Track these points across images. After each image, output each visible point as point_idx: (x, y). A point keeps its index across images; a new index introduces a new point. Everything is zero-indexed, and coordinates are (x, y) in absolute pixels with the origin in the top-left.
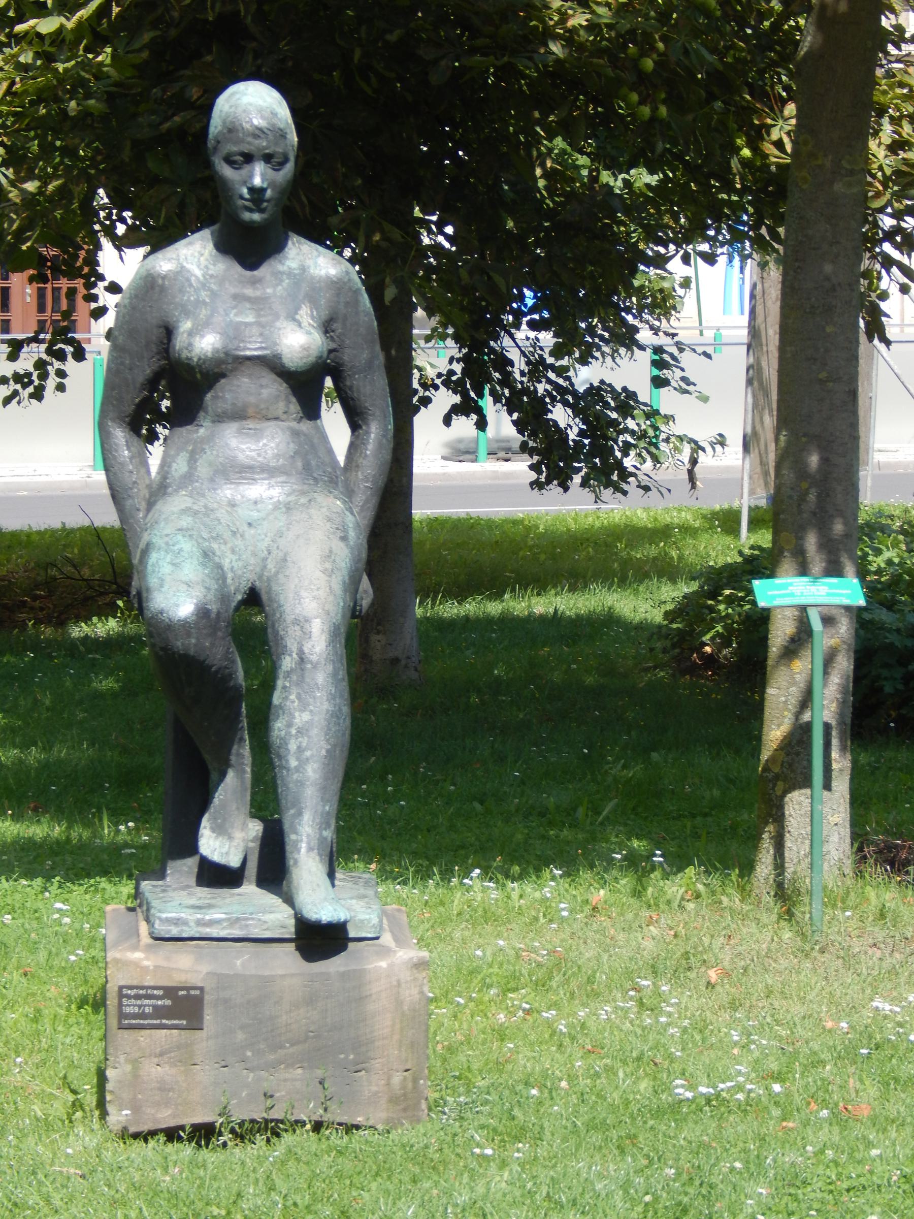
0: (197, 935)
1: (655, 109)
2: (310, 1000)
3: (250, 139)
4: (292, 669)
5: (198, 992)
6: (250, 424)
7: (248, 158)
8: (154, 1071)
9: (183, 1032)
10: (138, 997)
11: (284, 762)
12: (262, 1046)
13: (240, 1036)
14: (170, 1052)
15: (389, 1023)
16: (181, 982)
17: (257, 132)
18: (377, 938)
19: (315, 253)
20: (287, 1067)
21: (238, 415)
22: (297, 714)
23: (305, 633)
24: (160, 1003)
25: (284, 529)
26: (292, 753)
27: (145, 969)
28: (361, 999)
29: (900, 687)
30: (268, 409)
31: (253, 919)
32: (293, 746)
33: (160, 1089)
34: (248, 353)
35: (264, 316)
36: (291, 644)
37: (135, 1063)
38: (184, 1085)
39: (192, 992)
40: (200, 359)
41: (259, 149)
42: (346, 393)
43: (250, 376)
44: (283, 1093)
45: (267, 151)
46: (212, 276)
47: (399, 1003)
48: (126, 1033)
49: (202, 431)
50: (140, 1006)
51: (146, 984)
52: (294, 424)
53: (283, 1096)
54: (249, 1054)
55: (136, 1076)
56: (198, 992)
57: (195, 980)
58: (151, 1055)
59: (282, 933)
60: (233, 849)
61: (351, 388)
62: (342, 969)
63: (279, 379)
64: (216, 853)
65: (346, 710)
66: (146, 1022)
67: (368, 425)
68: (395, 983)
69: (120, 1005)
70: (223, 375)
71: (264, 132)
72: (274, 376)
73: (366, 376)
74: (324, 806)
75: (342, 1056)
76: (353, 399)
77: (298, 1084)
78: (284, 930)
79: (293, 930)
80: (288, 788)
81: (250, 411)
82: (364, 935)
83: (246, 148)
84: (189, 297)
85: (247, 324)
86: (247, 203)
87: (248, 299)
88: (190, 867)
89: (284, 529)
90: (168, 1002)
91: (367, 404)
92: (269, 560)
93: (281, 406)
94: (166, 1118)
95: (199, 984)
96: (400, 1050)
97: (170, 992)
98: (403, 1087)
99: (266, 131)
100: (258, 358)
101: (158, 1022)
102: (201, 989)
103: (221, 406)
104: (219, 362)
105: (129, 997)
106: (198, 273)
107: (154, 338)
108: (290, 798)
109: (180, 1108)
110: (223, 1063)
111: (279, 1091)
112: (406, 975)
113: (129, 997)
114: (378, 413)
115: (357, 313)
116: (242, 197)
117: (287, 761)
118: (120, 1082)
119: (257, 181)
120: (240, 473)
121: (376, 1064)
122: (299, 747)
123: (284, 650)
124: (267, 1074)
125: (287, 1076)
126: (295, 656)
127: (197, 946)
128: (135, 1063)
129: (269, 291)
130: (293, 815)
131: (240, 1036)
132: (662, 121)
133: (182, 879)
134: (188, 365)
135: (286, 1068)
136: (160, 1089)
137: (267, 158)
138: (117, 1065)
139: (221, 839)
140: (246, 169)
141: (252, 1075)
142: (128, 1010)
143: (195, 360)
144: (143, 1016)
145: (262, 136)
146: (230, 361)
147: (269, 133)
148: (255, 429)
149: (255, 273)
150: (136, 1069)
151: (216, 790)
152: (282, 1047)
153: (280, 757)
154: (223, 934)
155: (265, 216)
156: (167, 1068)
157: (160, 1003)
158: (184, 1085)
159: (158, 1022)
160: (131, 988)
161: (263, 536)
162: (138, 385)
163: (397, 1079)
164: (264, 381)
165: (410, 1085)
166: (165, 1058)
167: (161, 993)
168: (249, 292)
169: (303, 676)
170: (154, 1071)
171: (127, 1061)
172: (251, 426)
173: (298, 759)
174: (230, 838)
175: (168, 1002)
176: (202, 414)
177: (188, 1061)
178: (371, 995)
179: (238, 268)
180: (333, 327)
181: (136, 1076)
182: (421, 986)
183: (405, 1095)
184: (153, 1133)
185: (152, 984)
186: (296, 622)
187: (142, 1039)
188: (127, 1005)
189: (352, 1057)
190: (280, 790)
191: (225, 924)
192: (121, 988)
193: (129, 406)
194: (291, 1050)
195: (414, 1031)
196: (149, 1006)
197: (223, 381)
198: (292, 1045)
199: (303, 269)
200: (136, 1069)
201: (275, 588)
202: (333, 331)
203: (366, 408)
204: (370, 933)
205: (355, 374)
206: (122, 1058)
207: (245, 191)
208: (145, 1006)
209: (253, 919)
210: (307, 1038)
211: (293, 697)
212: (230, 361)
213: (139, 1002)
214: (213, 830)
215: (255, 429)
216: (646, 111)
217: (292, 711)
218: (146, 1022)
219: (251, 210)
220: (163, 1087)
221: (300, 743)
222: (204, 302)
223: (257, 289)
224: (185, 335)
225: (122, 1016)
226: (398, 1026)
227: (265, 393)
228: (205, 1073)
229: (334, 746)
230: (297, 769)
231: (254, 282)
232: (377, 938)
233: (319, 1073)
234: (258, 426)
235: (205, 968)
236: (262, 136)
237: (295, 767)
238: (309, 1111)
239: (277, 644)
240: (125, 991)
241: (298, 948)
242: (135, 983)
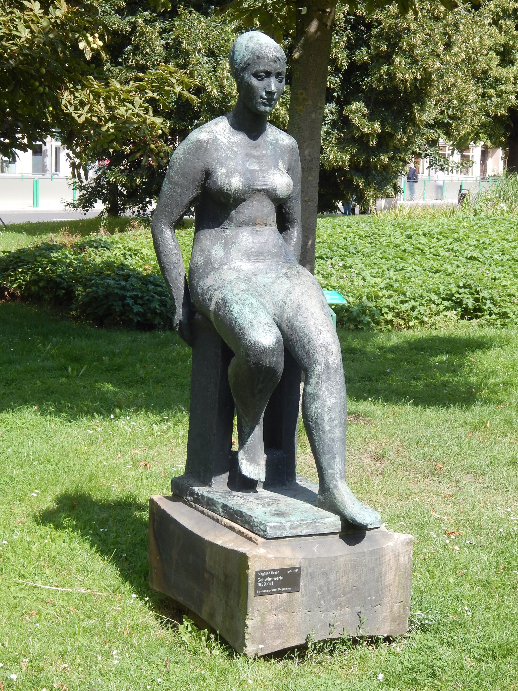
0: (290, 535)
1: (44, 89)
2: (355, 568)
3: (271, 63)
4: (322, 373)
5: (297, 570)
6: (257, 228)
7: (268, 74)
8: (272, 619)
9: (288, 594)
10: (266, 577)
11: (321, 428)
12: (329, 598)
13: (318, 593)
14: (282, 606)
15: (393, 577)
16: (288, 565)
17: (276, 59)
18: (379, 528)
19: (278, 132)
21: (251, 223)
22: (328, 399)
23: (329, 352)
24: (277, 579)
25: (291, 289)
26: (326, 422)
27: (270, 559)
28: (380, 565)
29: (122, 309)
31: (319, 522)
32: (326, 418)
33: (275, 629)
34: (259, 188)
35: (263, 166)
36: (321, 359)
37: (263, 615)
38: (288, 625)
39: (295, 571)
40: (235, 191)
41: (275, 70)
42: (286, 210)
44: (339, 623)
46: (233, 143)
47: (398, 565)
48: (258, 598)
49: (228, 232)
50: (266, 582)
51: (270, 568)
53: (339, 625)
54: (322, 602)
55: (263, 623)
56: (297, 570)
57: (296, 563)
58: (271, 610)
59: (334, 530)
60: (261, 471)
61: (289, 208)
62: (371, 549)
63: (272, 202)
64: (252, 474)
66: (270, 591)
67: (293, 228)
68: (397, 554)
69: (256, 582)
70: (245, 200)
71: (279, 60)
75: (369, 598)
76: (289, 214)
77: (347, 617)
78: (335, 528)
79: (340, 527)
80: (324, 442)
81: (258, 221)
82: (374, 527)
83: (268, 68)
84: (221, 155)
85: (255, 171)
86: (264, 101)
87: (254, 156)
88: (224, 479)
89: (291, 289)
90: (282, 578)
92: (286, 307)
94: (278, 645)
95: (298, 566)
96: (398, 592)
97: (283, 572)
98: (399, 612)
99: (280, 59)
100: (263, 190)
101: (276, 590)
102: (299, 568)
103: (242, 218)
104: (245, 192)
105: (261, 577)
106: (225, 141)
107: (198, 178)
108: (326, 448)
109: (286, 638)
110: (309, 610)
111: (337, 622)
112: (402, 549)
113: (261, 577)
116: (262, 97)
117: (323, 427)
118: (254, 627)
119: (273, 88)
120: (257, 256)
121: (386, 600)
122: (330, 419)
123: (316, 362)
124: (331, 613)
125: (342, 613)
126: (323, 365)
127: (289, 541)
128: (263, 615)
129: (264, 152)
130: (329, 458)
131: (318, 593)
132: (46, 94)
133: (221, 486)
134: (228, 194)
136: (275, 629)
138: (253, 618)
139: (253, 465)
140: (266, 81)
141: (323, 614)
142: (260, 585)
143: (233, 191)
144: (268, 587)
145: (278, 62)
148: (259, 231)
150: (263, 618)
151: (249, 437)
152: (340, 597)
153: (317, 424)
154: (304, 533)
156: (279, 616)
157: (277, 579)
158: (288, 625)
159: (276, 590)
160: (262, 572)
161: (278, 293)
162: (184, 204)
163: (396, 608)
164: (265, 204)
165: (402, 610)
166: (279, 610)
167: (278, 573)
168: (254, 152)
169: (329, 377)
170: (272, 619)
171: (259, 615)
172: (257, 229)
173: (330, 425)
174: (258, 464)
175: (282, 578)
176: (227, 222)
177: (290, 610)
179: (247, 138)
181: (263, 623)
182: (409, 555)
183: (399, 616)
184: (269, 655)
185: (273, 568)
186: (322, 345)
187: (267, 601)
188: (260, 582)
189: (374, 598)
190: (317, 443)
191: (304, 527)
192: (257, 572)
193: (176, 216)
194: (344, 598)
195: (405, 580)
196: (271, 581)
197: (244, 203)
198: (344, 595)
199: (276, 140)
200: (263, 618)
201: (296, 324)
206: (256, 613)
207: (264, 93)
208: (269, 581)
209: (319, 522)
210: (352, 590)
211: (324, 389)
213: (266, 580)
214: (248, 460)
215: (259, 231)
216: (41, 89)
217: (325, 397)
218: (270, 591)
219: (265, 105)
220: (277, 627)
221: (331, 416)
222: (231, 158)
223: (258, 151)
224: (224, 177)
225: (257, 588)
226: (397, 578)
227: (266, 210)
228: (299, 617)
230: (330, 432)
231: (256, 147)
232: (379, 528)
233: (358, 609)
234: (261, 229)
235: (300, 555)
236: (278, 62)
237: (329, 430)
238: (352, 632)
239: (309, 357)
240: (259, 574)
241: (341, 537)
242: (264, 568)
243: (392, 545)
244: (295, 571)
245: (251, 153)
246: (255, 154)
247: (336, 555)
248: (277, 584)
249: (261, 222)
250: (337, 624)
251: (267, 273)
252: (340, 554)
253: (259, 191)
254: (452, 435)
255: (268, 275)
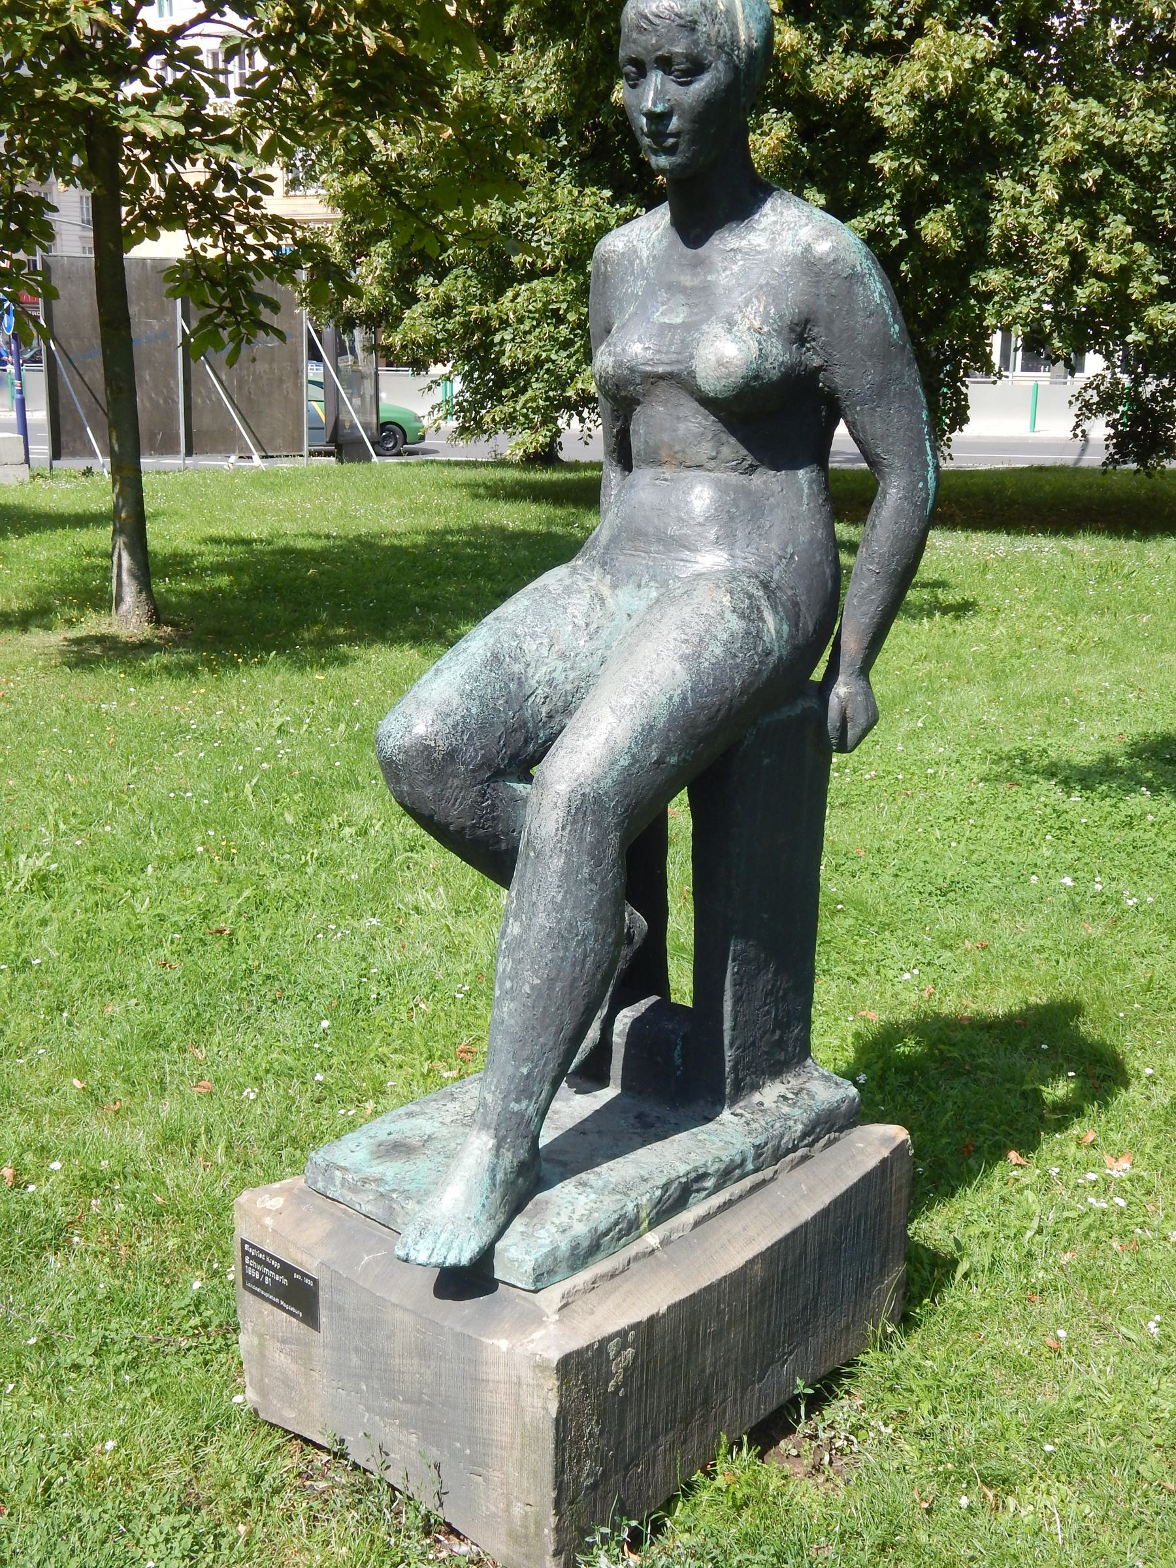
20: (401, 1425)
28: (478, 1381)
30: (684, 452)
39: (307, 1281)
43: (665, 403)
45: (660, 53)
50: (261, 1273)
52: (734, 478)
63: (702, 409)
65: (586, 926)
72: (696, 405)
73: (874, 409)
74: (517, 1068)
81: (664, 454)
87: (683, 290)
91: (879, 451)
93: (706, 449)
97: (286, 1269)
101: (277, 1300)
114: (897, 463)
115: (851, 313)
135: (401, 1425)
137: (665, 64)
146: (638, 381)
147: (657, 21)
149: (700, 250)
155: (677, 159)
159: (277, 1300)
172: (667, 476)
178: (488, 1381)
180: (813, 333)
198: (405, 1401)
202: (814, 340)
203: (878, 455)
204: (521, 1281)
205: (855, 405)
212: (638, 381)
229: (551, 981)
243: (504, 1349)
244: (307, 1281)
245: (679, 282)
246: (688, 284)
247: (386, 1296)
248: (276, 1289)
249: (669, 456)
250: (499, 1452)
251: (639, 586)
252: (394, 1299)
253: (661, 377)
254: (22, 1110)
255: (642, 591)
